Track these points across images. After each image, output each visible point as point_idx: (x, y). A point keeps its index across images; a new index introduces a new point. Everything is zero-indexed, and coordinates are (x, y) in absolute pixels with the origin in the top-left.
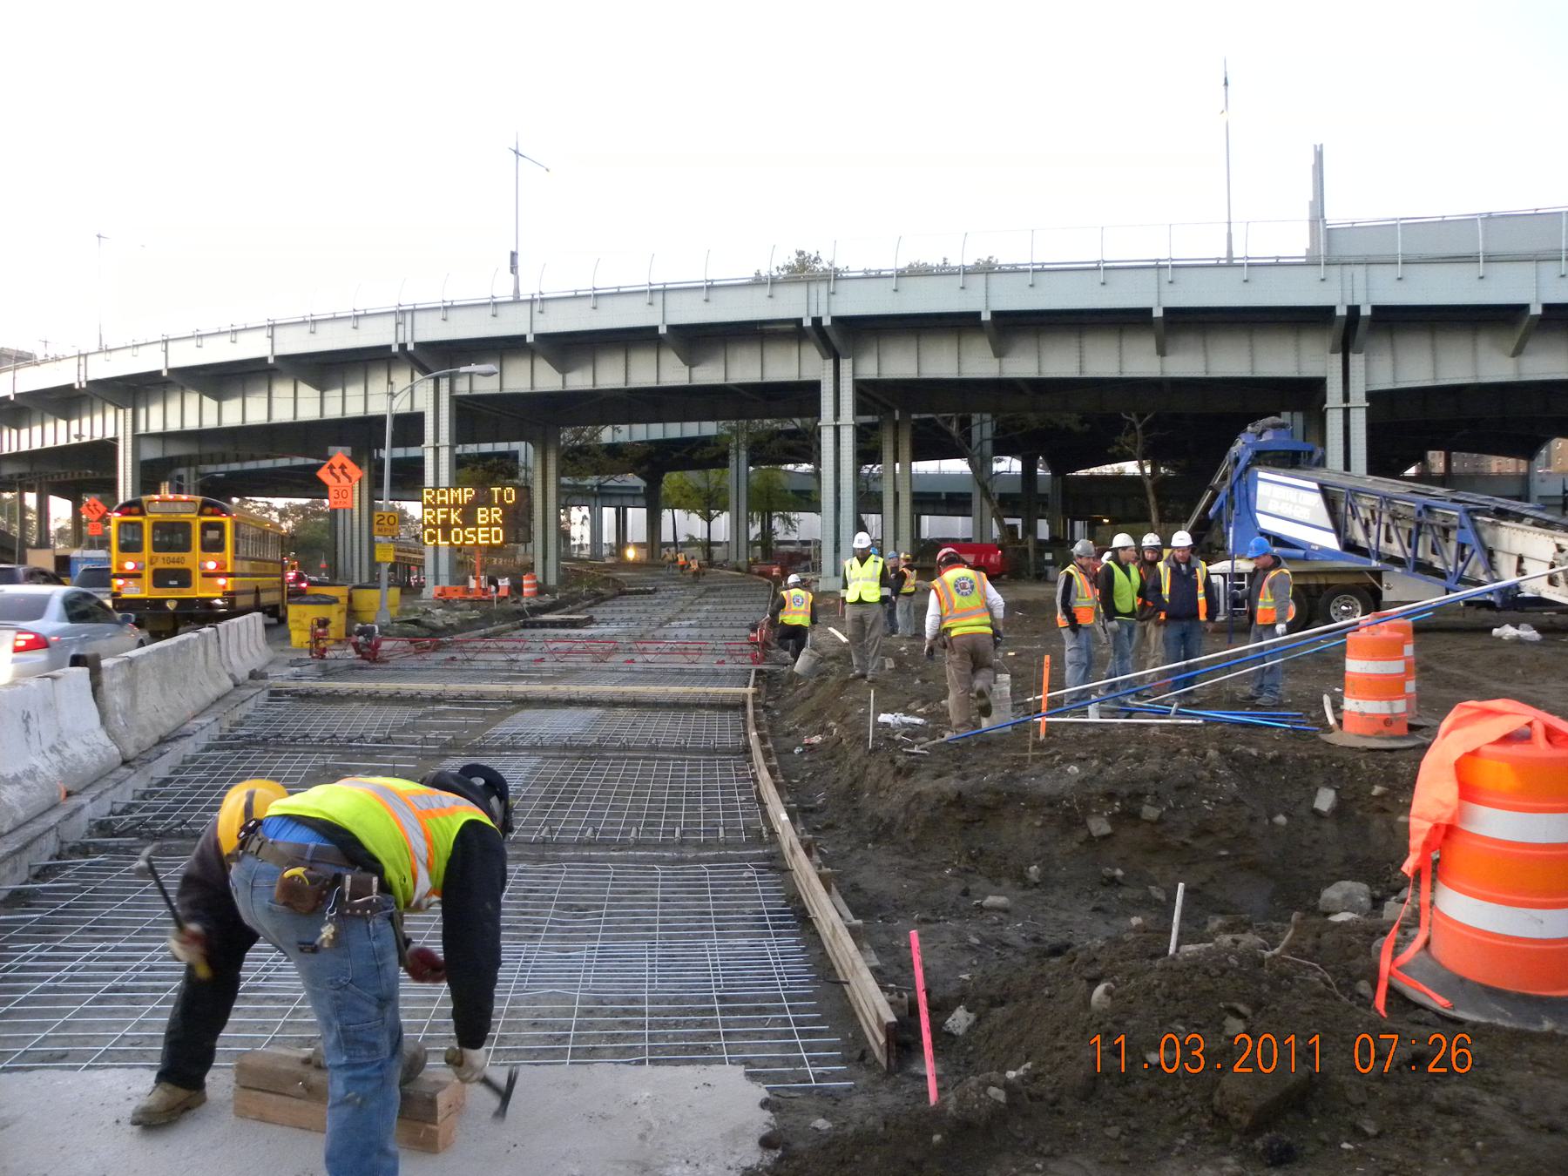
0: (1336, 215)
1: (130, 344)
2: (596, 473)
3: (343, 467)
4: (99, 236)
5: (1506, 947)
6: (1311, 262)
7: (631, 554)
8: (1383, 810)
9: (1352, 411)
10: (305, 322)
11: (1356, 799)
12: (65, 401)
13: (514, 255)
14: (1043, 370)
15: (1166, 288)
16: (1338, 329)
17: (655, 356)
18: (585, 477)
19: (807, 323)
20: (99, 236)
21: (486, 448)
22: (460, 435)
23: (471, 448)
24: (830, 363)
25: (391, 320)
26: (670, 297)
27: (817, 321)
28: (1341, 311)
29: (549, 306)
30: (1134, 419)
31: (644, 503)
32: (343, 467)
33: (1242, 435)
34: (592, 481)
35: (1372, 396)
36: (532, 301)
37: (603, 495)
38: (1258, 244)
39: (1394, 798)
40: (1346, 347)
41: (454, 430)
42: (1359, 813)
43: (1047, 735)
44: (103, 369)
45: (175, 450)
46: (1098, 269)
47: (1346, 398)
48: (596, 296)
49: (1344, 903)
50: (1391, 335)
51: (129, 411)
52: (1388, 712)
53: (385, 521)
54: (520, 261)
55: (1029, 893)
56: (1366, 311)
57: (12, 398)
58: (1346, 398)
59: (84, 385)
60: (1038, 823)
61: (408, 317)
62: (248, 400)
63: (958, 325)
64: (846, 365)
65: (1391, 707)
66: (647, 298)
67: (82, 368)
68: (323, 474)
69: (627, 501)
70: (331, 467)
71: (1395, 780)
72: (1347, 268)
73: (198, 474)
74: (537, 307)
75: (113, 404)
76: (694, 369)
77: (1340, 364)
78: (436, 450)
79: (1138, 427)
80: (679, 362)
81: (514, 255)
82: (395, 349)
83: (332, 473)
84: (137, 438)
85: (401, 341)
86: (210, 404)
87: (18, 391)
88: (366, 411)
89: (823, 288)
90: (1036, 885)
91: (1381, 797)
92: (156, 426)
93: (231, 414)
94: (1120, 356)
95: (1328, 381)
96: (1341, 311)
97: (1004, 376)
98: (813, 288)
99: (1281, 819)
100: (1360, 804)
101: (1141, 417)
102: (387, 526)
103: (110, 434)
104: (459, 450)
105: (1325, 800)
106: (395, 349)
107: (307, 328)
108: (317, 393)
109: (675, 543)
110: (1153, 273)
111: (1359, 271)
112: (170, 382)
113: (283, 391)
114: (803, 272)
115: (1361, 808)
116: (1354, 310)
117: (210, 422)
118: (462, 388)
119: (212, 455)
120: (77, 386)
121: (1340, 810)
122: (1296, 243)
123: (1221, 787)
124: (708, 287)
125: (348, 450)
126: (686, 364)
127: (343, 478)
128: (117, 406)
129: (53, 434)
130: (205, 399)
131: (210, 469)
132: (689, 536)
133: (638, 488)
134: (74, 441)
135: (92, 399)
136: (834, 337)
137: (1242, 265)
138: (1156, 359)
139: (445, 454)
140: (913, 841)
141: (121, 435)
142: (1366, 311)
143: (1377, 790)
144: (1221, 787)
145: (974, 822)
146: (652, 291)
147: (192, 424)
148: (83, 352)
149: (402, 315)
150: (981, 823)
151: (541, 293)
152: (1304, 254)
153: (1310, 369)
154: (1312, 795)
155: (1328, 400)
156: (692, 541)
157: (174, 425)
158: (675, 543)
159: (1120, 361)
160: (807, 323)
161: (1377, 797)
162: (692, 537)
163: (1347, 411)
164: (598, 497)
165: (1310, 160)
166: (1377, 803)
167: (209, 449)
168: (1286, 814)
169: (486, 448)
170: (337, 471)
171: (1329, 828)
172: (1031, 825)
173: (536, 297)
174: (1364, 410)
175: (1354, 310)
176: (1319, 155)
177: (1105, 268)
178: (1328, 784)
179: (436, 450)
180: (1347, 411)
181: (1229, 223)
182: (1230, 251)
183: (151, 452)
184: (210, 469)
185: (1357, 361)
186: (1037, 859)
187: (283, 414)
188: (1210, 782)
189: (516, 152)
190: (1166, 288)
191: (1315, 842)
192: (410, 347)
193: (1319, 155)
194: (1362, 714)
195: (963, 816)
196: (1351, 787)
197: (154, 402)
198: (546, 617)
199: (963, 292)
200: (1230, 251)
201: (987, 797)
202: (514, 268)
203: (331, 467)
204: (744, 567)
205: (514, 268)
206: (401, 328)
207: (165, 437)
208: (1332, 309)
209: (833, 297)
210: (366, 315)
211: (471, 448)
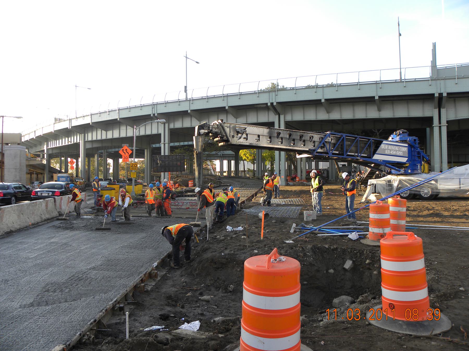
0: (440, 63)
1: (82, 116)
2: (215, 151)
3: (126, 150)
4: (76, 86)
5: (248, 350)
6: (432, 79)
7: (232, 175)
8: (369, 269)
9: (442, 127)
10: (128, 108)
11: (361, 264)
12: (67, 132)
13: (186, 87)
14: (342, 117)
15: (379, 89)
16: (436, 101)
17: (226, 116)
18: (212, 151)
19: (269, 104)
20: (76, 86)
21: (182, 144)
22: (171, 140)
23: (177, 144)
24: (277, 116)
25: (151, 107)
26: (229, 98)
27: (272, 104)
28: (437, 95)
29: (195, 102)
30: (376, 131)
31: (234, 159)
32: (126, 150)
33: (392, 136)
34: (214, 153)
35: (448, 122)
36: (190, 100)
37: (223, 157)
38: (410, 75)
39: (373, 265)
40: (440, 107)
41: (169, 138)
42: (361, 269)
43: (264, 237)
44: (75, 123)
45: (95, 145)
46: (357, 85)
47: (440, 123)
48: (208, 98)
49: (339, 305)
50: (455, 101)
51: (83, 135)
52: (382, 232)
53: (134, 166)
54: (188, 88)
55: (226, 294)
56: (445, 95)
57: (53, 132)
58: (440, 123)
59: (70, 128)
60: (238, 270)
61: (155, 106)
62: (114, 131)
63: (316, 103)
64: (282, 117)
65: (383, 231)
66: (222, 98)
67: (70, 123)
68: (121, 152)
69: (231, 158)
70: (123, 150)
71: (374, 258)
72: (438, 81)
73: (107, 152)
74: (191, 102)
75: (79, 133)
76: (237, 119)
77: (438, 112)
78: (164, 144)
79: (378, 134)
80: (233, 117)
81: (186, 87)
82: (152, 115)
83: (123, 152)
84: (85, 142)
85: (154, 113)
86: (104, 132)
87: (55, 130)
88: (145, 133)
89: (274, 94)
90: (230, 292)
91: (369, 264)
92: (90, 139)
93: (110, 135)
94: (366, 110)
95: (434, 118)
96: (437, 95)
97: (330, 119)
98: (271, 94)
99: (331, 271)
100: (362, 266)
101: (379, 130)
102: (134, 167)
103: (78, 141)
104: (172, 144)
105: (348, 264)
106: (152, 115)
107: (128, 110)
108: (235, 119)
109: (244, 171)
110: (375, 85)
111: (442, 81)
112: (153, 118)
113: (123, 128)
114: (274, 89)
115: (363, 268)
116: (441, 94)
117: (104, 137)
118: (172, 126)
119: (105, 147)
120: (69, 128)
121: (354, 268)
122: (426, 73)
123: (306, 259)
124: (240, 95)
125: (128, 145)
126: (235, 118)
127: (126, 153)
128: (80, 134)
129: (64, 142)
130: (103, 131)
131: (110, 150)
132: (248, 169)
133: (234, 154)
134: (70, 143)
135: (74, 132)
136: (279, 109)
137: (404, 82)
138: (378, 112)
139: (167, 145)
140: (196, 274)
141: (81, 142)
142: (445, 95)
143: (368, 261)
144: (306, 259)
145: (219, 268)
146: (224, 96)
147: (99, 138)
148: (71, 118)
149: (154, 105)
150: (221, 269)
151: (192, 98)
152: (429, 77)
153: (427, 113)
154: (344, 263)
155: (434, 124)
156: (249, 170)
157: (94, 138)
158: (244, 171)
159: (366, 113)
160: (269, 104)
161: (367, 264)
162: (249, 169)
163: (440, 127)
164: (222, 158)
165: (431, 47)
166: (367, 266)
167: (109, 145)
168: (334, 269)
169: (182, 144)
170: (125, 151)
171: (348, 274)
172: (237, 270)
173: (191, 99)
174: (446, 127)
175: (441, 94)
176: (434, 45)
177: (360, 84)
178: (351, 259)
179: (164, 144)
180: (440, 127)
181: (401, 69)
182: (401, 77)
183: (89, 146)
184: (110, 150)
185: (443, 111)
186: (235, 282)
187: (123, 135)
188: (303, 257)
189: (186, 57)
190: (379, 89)
191: (342, 280)
192: (156, 115)
193: (434, 45)
194: (373, 233)
195: (215, 266)
196: (359, 260)
197: (90, 132)
198: (189, 194)
199: (316, 93)
200: (401, 77)
201: (224, 260)
202: (186, 91)
203: (123, 150)
204: (260, 178)
205: (186, 91)
206: (153, 109)
207: (92, 141)
208: (434, 94)
209: (276, 96)
210: (144, 106)
211: (177, 144)
